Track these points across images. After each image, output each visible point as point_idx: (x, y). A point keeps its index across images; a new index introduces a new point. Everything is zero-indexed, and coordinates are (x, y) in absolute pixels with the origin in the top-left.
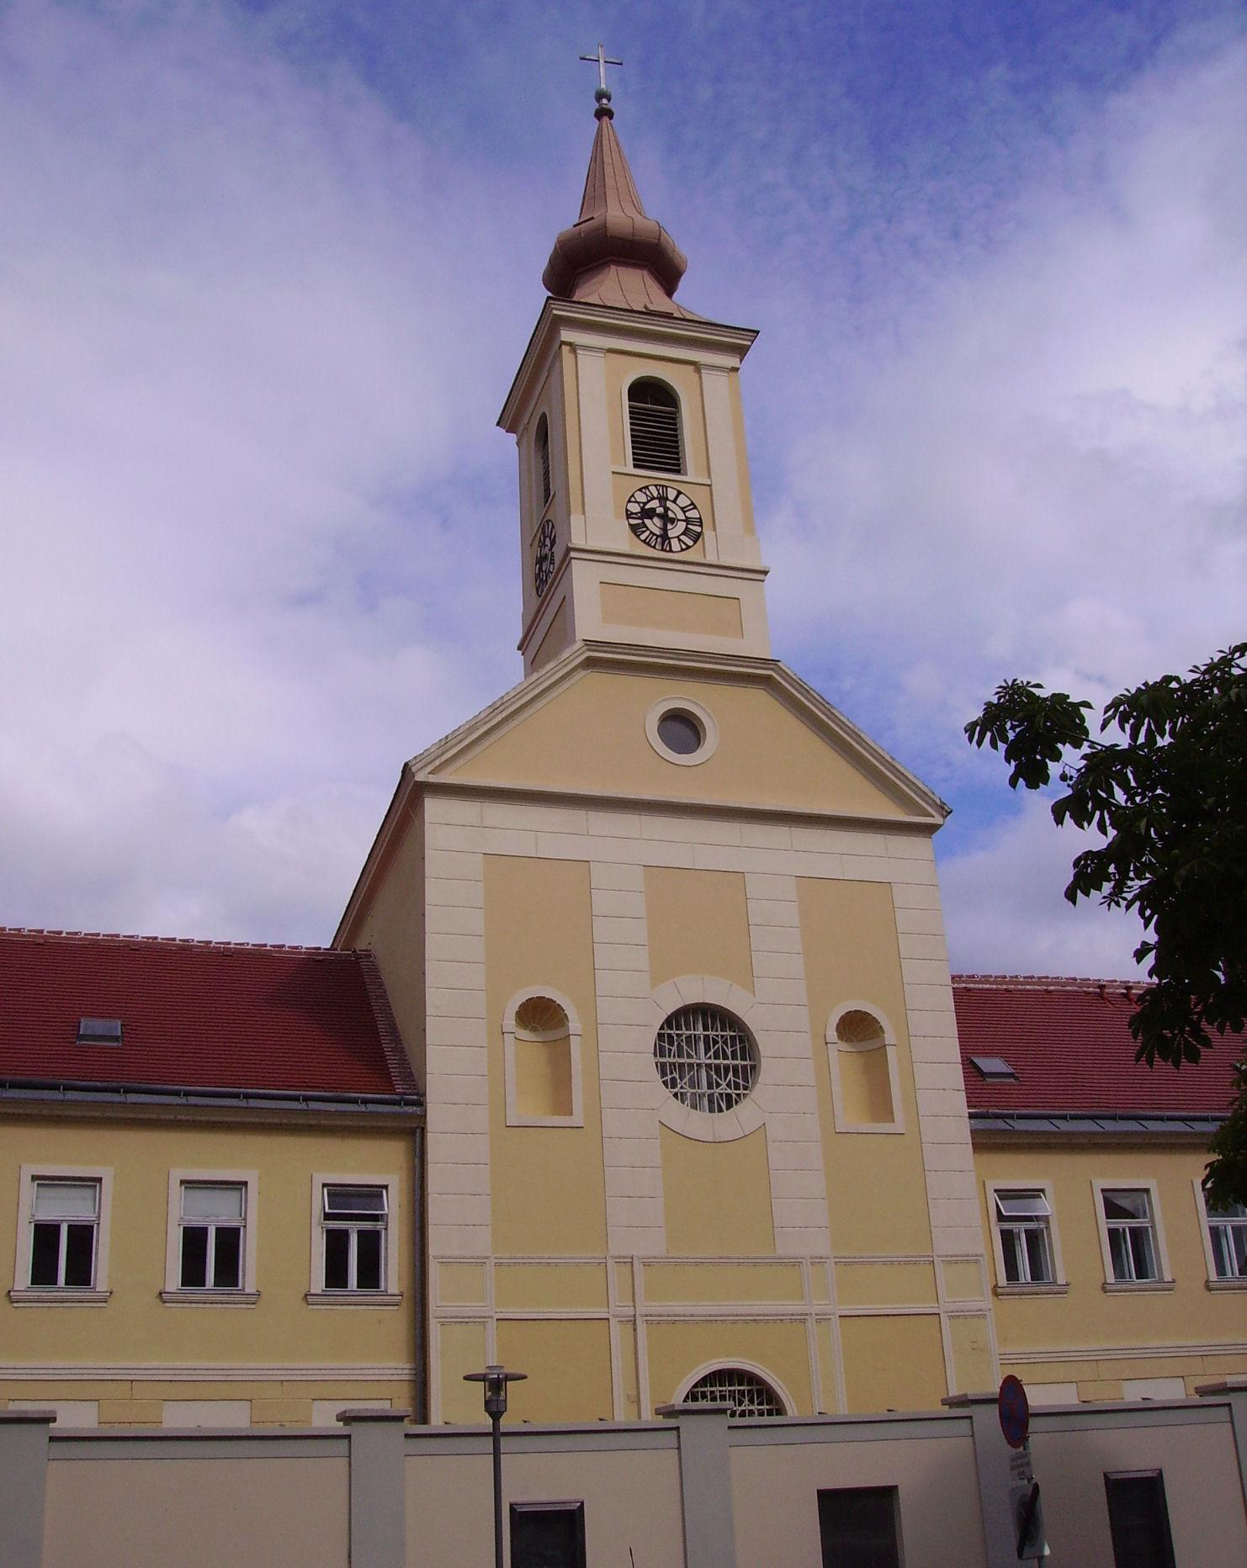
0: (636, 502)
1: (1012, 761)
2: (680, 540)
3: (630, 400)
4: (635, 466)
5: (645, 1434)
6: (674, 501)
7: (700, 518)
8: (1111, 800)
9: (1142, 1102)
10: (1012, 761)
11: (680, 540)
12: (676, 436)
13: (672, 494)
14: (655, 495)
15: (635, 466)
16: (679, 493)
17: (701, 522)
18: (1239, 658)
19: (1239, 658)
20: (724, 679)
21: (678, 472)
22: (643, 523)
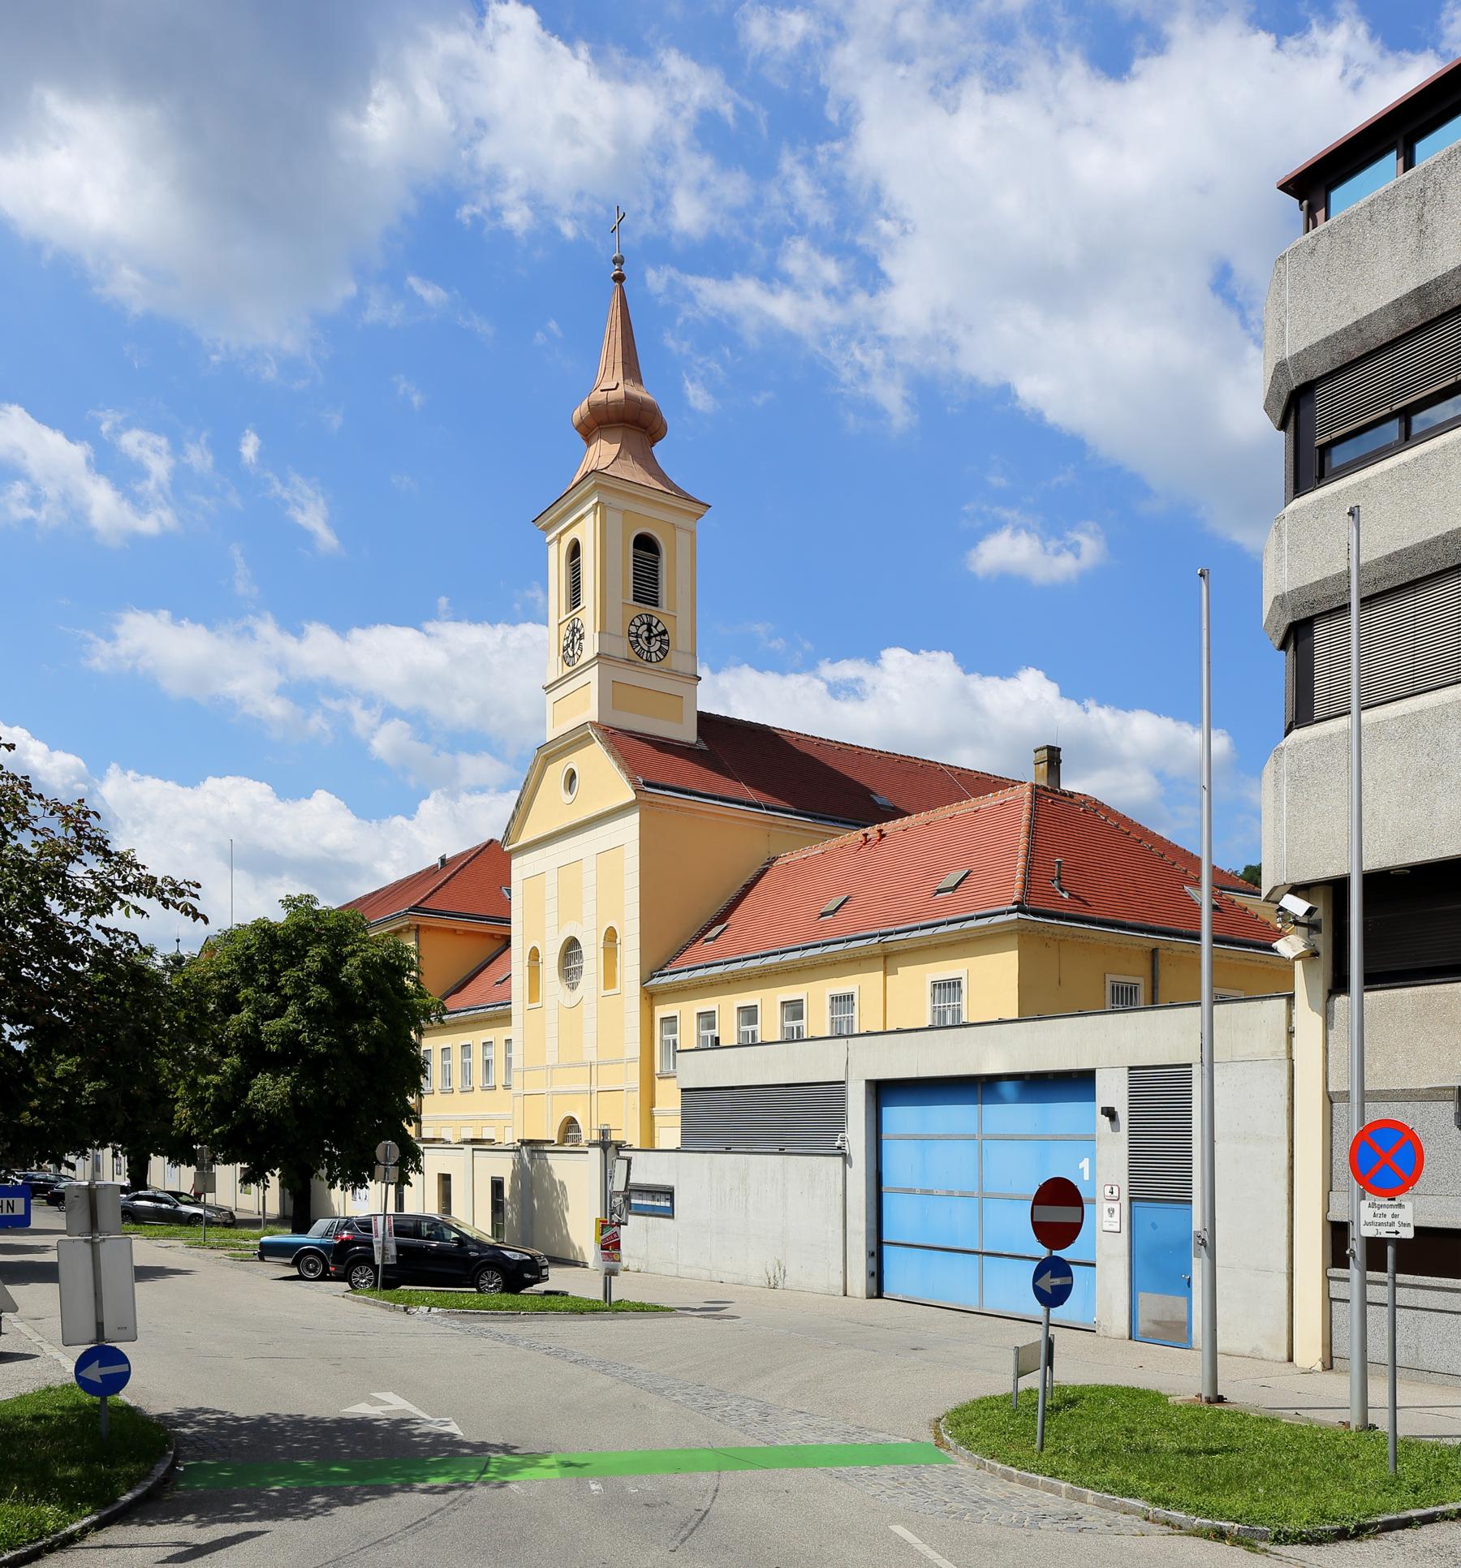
0: (636, 626)
1: (1080, 1167)
2: (656, 654)
3: (634, 547)
4: (634, 600)
5: (840, 1210)
6: (655, 627)
7: (668, 640)
8: (335, 1445)
9: (1051, 893)
10: (1080, 1167)
11: (656, 654)
12: (657, 567)
13: (655, 622)
14: (646, 621)
15: (634, 600)
16: (659, 621)
17: (668, 643)
18: (391, 1165)
19: (391, 1165)
20: (1213, 1369)
21: (657, 606)
22: (637, 640)
